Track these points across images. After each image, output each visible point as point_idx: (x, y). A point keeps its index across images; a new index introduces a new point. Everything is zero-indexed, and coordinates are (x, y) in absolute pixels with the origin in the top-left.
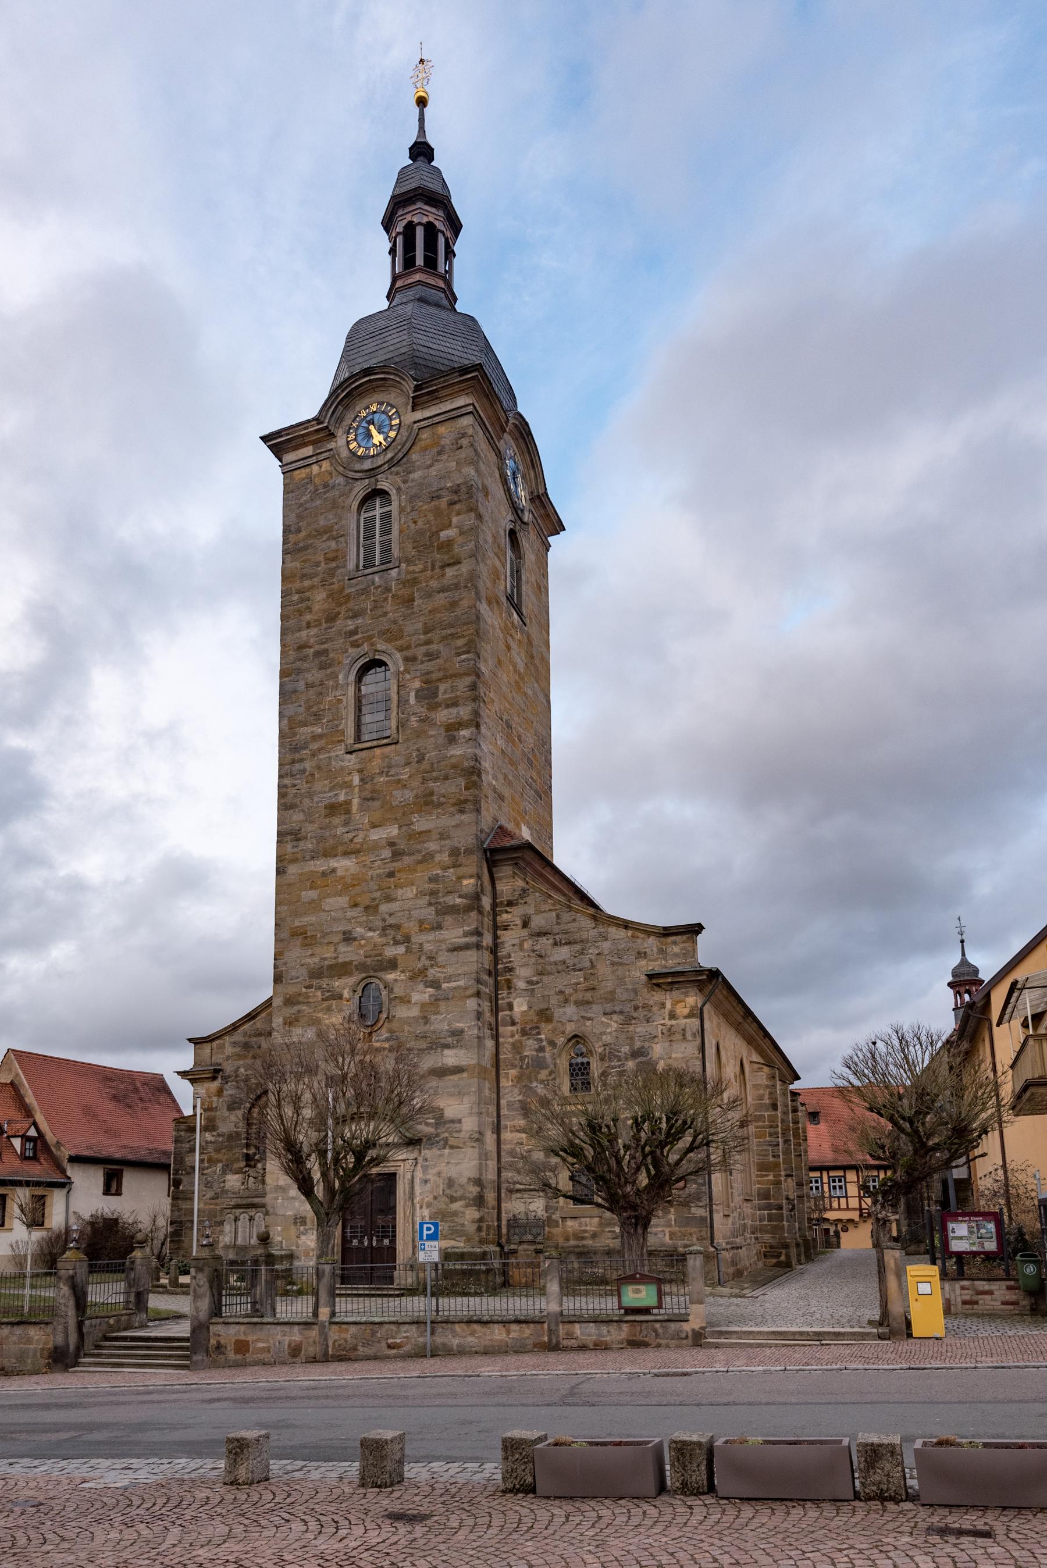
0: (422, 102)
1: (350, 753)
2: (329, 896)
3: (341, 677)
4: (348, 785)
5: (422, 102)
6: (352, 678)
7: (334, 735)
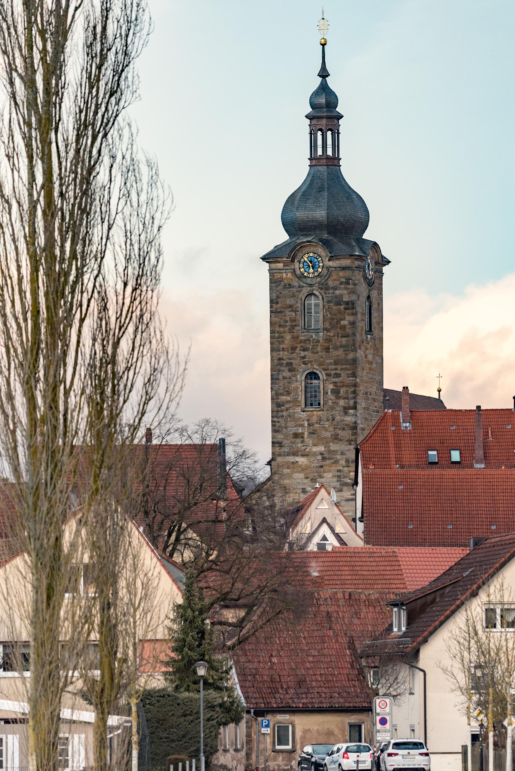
0: (323, 45)
1: (304, 411)
2: (295, 472)
3: (298, 376)
4: (302, 426)
5: (323, 45)
6: (303, 378)
7: (295, 402)
